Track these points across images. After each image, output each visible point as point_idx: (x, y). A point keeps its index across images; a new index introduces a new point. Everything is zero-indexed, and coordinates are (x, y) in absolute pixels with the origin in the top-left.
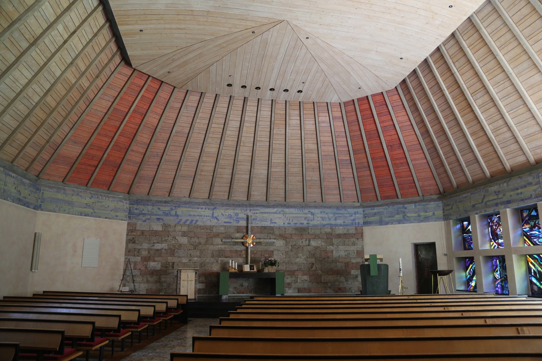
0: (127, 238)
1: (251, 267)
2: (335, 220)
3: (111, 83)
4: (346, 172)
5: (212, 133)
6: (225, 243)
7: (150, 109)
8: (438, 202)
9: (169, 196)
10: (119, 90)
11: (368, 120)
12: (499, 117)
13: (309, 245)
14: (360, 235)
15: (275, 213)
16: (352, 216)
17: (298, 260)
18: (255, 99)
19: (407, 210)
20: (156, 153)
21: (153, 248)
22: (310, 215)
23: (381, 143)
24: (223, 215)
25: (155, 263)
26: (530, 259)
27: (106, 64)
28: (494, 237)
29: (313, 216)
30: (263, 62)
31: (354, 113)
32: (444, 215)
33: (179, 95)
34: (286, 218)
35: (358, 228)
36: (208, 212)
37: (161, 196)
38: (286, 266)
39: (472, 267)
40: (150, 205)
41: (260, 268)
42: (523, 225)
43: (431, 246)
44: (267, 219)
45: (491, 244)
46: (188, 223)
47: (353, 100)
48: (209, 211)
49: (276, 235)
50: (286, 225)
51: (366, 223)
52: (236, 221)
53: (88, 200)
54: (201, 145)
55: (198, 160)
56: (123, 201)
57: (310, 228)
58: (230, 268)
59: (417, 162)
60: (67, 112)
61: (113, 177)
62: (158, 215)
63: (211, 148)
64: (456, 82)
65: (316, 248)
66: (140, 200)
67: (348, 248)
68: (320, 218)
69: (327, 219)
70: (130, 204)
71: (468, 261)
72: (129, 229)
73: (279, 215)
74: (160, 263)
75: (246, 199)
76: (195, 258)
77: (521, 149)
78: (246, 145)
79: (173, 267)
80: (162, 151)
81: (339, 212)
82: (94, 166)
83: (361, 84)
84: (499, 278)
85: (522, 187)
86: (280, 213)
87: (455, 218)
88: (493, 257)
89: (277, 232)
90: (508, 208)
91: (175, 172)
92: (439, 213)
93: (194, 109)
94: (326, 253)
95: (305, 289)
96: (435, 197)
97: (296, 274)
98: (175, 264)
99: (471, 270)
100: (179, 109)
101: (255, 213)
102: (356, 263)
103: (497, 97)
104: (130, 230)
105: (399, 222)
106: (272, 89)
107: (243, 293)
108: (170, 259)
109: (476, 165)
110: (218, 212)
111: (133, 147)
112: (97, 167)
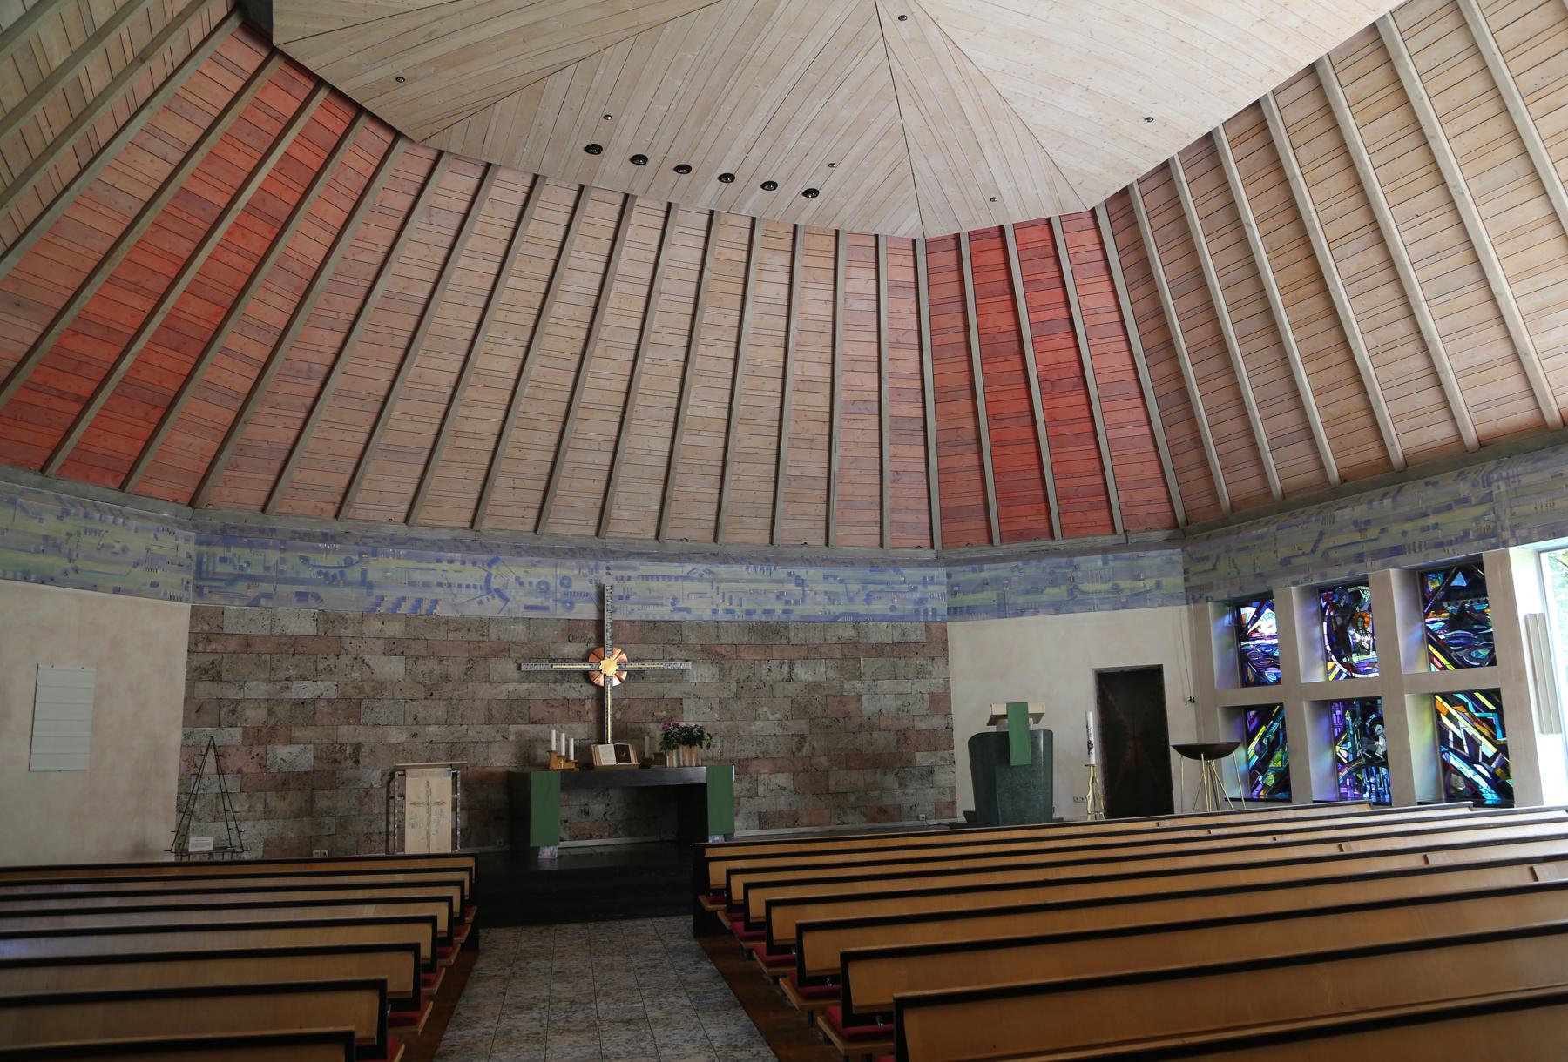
0: (189, 662)
1: (621, 753)
2: (868, 600)
3: (182, 93)
4: (906, 456)
5: (505, 307)
6: (528, 676)
7: (306, 206)
8: (1170, 551)
9: (336, 516)
10: (206, 124)
11: (994, 299)
12: (1400, 311)
13: (790, 680)
14: (938, 647)
15: (685, 578)
16: (915, 589)
17: (757, 726)
18: (659, 207)
19: (1080, 574)
20: (305, 366)
21: (286, 695)
22: (791, 587)
23: (1025, 370)
24: (521, 584)
25: (295, 749)
26: (1445, 704)
27: (180, 14)
28: (1335, 647)
29: (801, 588)
30: (732, 81)
31: (954, 276)
32: (1186, 589)
33: (407, 164)
34: (720, 595)
35: (933, 626)
36: (474, 575)
37: (308, 516)
38: (722, 746)
39: (1265, 734)
40: (274, 548)
41: (647, 756)
42: (1427, 615)
43: (1150, 678)
44: (661, 598)
45: (1329, 669)
46: (405, 609)
47: (957, 237)
48: (477, 568)
49: (691, 647)
50: (721, 616)
51: (956, 612)
52: (565, 602)
53: (50, 525)
54: (466, 345)
55: (447, 397)
56: (177, 531)
57: (792, 626)
58: (554, 757)
59: (1121, 433)
60: (9, 181)
61: (142, 444)
62: (303, 582)
63: (497, 358)
64: (1292, 203)
65: (813, 687)
66: (233, 527)
67: (905, 686)
68: (822, 596)
69: (844, 599)
70: (200, 543)
71: (1255, 716)
72: (198, 630)
73: (696, 586)
74: (311, 747)
75: (593, 533)
76: (431, 729)
77: (1446, 404)
78: (615, 354)
79: (357, 762)
80: (329, 359)
81: (878, 576)
82: (78, 399)
83: (1004, 186)
84: (1351, 759)
85: (1438, 511)
86: (700, 579)
87: (1225, 597)
88: (1332, 702)
89: (693, 640)
90: (1394, 567)
91: (366, 435)
92: (1175, 582)
93: (455, 221)
94: (841, 701)
95: (780, 815)
96: (1160, 535)
97: (752, 769)
98: (365, 750)
99: (1265, 741)
100: (403, 215)
101: (622, 578)
102: (929, 731)
103: (1404, 256)
104: (202, 633)
105: (1058, 607)
106: (727, 178)
107: (591, 837)
108: (346, 733)
109: (1302, 448)
110: (507, 574)
111: (227, 339)
112: (88, 402)
